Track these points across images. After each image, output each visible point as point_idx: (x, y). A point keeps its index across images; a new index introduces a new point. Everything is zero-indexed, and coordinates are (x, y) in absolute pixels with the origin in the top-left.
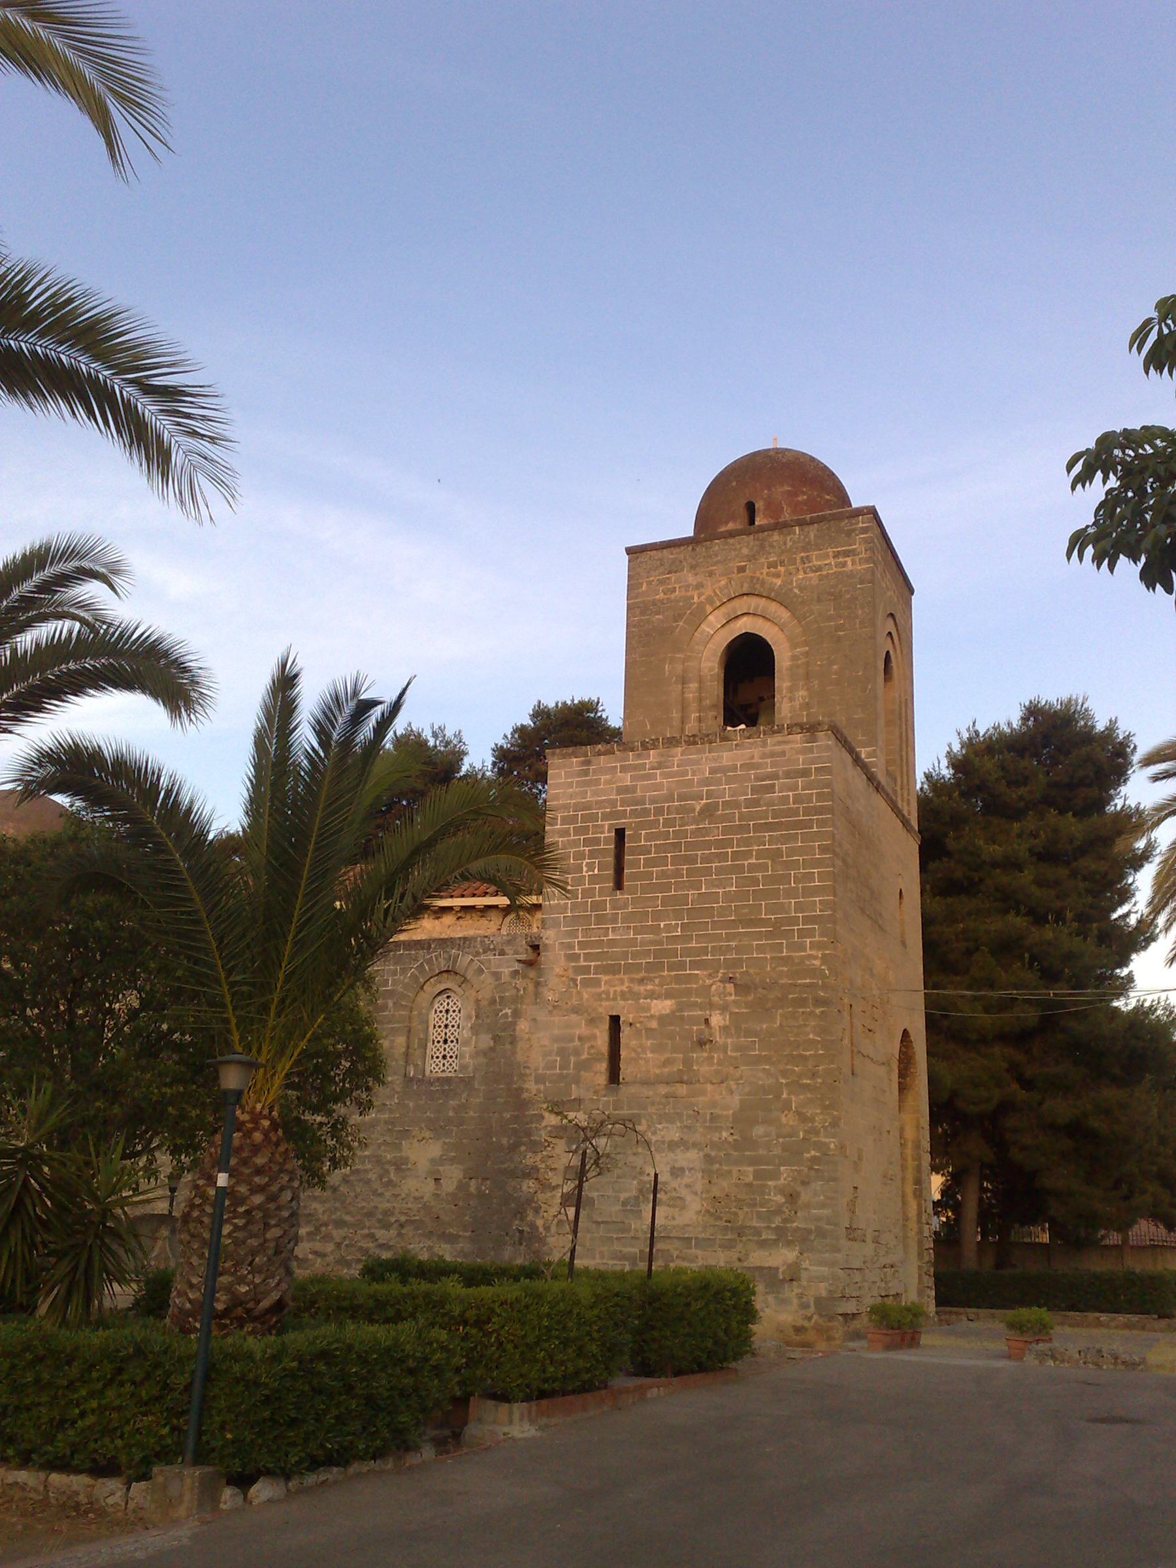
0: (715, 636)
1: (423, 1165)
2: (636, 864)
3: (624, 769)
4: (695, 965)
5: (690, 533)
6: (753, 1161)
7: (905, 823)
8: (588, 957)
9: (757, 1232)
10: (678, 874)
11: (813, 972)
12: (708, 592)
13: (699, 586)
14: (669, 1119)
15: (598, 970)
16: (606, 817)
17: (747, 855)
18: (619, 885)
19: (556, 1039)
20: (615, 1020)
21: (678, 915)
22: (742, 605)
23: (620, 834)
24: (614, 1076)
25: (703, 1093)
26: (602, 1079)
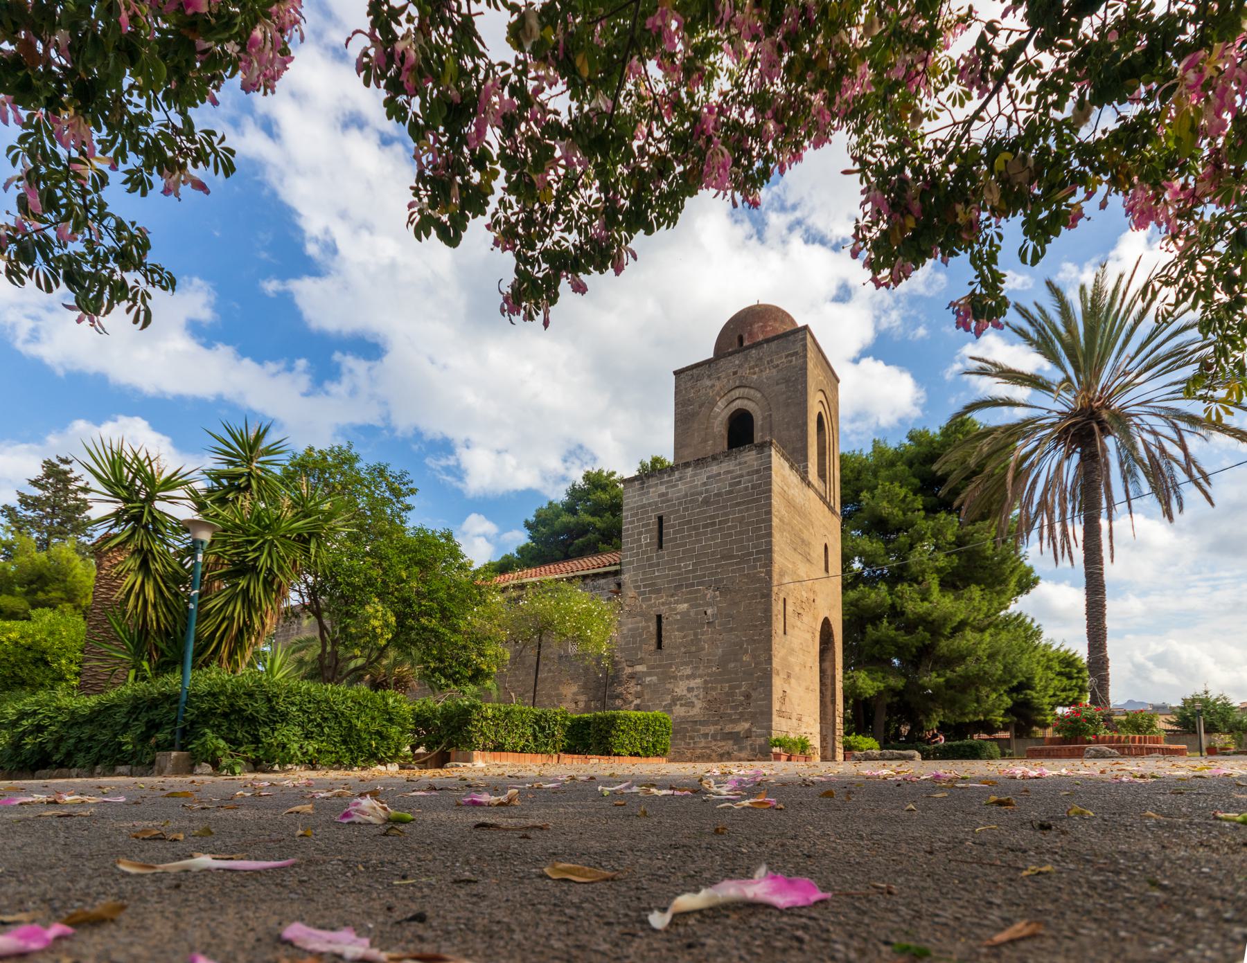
0: (722, 412)
1: (570, 696)
2: (668, 534)
3: (662, 484)
4: (699, 584)
5: (711, 355)
6: (728, 681)
7: (832, 509)
8: (645, 586)
9: (730, 715)
10: (690, 536)
11: (760, 580)
12: (717, 388)
13: (713, 386)
14: (686, 664)
15: (650, 592)
16: (653, 511)
17: (727, 521)
18: (660, 547)
19: (630, 630)
20: (659, 618)
21: (691, 558)
22: (737, 393)
23: (660, 519)
24: (659, 646)
25: (703, 649)
26: (653, 648)
